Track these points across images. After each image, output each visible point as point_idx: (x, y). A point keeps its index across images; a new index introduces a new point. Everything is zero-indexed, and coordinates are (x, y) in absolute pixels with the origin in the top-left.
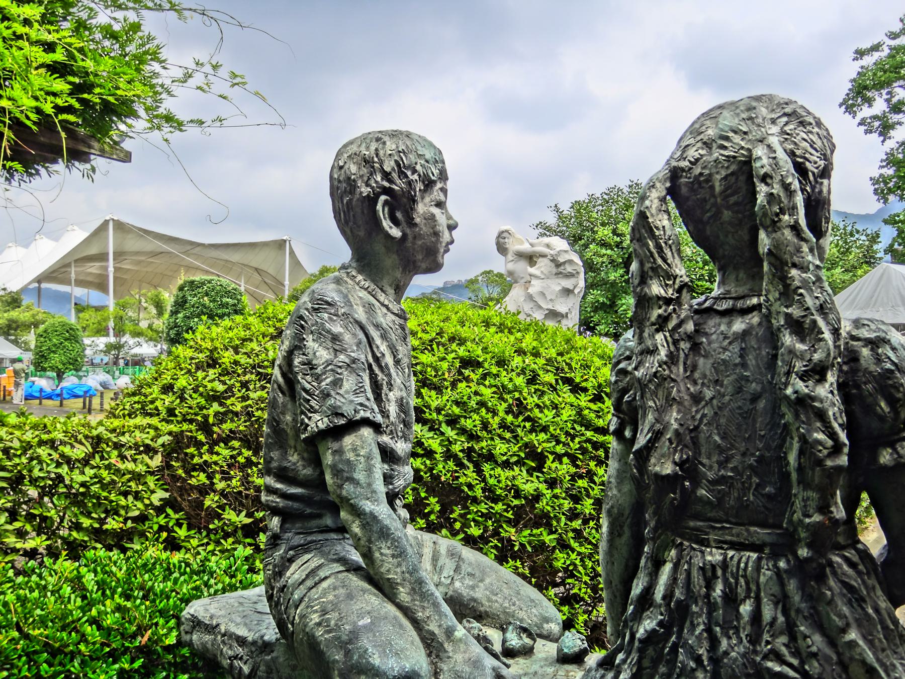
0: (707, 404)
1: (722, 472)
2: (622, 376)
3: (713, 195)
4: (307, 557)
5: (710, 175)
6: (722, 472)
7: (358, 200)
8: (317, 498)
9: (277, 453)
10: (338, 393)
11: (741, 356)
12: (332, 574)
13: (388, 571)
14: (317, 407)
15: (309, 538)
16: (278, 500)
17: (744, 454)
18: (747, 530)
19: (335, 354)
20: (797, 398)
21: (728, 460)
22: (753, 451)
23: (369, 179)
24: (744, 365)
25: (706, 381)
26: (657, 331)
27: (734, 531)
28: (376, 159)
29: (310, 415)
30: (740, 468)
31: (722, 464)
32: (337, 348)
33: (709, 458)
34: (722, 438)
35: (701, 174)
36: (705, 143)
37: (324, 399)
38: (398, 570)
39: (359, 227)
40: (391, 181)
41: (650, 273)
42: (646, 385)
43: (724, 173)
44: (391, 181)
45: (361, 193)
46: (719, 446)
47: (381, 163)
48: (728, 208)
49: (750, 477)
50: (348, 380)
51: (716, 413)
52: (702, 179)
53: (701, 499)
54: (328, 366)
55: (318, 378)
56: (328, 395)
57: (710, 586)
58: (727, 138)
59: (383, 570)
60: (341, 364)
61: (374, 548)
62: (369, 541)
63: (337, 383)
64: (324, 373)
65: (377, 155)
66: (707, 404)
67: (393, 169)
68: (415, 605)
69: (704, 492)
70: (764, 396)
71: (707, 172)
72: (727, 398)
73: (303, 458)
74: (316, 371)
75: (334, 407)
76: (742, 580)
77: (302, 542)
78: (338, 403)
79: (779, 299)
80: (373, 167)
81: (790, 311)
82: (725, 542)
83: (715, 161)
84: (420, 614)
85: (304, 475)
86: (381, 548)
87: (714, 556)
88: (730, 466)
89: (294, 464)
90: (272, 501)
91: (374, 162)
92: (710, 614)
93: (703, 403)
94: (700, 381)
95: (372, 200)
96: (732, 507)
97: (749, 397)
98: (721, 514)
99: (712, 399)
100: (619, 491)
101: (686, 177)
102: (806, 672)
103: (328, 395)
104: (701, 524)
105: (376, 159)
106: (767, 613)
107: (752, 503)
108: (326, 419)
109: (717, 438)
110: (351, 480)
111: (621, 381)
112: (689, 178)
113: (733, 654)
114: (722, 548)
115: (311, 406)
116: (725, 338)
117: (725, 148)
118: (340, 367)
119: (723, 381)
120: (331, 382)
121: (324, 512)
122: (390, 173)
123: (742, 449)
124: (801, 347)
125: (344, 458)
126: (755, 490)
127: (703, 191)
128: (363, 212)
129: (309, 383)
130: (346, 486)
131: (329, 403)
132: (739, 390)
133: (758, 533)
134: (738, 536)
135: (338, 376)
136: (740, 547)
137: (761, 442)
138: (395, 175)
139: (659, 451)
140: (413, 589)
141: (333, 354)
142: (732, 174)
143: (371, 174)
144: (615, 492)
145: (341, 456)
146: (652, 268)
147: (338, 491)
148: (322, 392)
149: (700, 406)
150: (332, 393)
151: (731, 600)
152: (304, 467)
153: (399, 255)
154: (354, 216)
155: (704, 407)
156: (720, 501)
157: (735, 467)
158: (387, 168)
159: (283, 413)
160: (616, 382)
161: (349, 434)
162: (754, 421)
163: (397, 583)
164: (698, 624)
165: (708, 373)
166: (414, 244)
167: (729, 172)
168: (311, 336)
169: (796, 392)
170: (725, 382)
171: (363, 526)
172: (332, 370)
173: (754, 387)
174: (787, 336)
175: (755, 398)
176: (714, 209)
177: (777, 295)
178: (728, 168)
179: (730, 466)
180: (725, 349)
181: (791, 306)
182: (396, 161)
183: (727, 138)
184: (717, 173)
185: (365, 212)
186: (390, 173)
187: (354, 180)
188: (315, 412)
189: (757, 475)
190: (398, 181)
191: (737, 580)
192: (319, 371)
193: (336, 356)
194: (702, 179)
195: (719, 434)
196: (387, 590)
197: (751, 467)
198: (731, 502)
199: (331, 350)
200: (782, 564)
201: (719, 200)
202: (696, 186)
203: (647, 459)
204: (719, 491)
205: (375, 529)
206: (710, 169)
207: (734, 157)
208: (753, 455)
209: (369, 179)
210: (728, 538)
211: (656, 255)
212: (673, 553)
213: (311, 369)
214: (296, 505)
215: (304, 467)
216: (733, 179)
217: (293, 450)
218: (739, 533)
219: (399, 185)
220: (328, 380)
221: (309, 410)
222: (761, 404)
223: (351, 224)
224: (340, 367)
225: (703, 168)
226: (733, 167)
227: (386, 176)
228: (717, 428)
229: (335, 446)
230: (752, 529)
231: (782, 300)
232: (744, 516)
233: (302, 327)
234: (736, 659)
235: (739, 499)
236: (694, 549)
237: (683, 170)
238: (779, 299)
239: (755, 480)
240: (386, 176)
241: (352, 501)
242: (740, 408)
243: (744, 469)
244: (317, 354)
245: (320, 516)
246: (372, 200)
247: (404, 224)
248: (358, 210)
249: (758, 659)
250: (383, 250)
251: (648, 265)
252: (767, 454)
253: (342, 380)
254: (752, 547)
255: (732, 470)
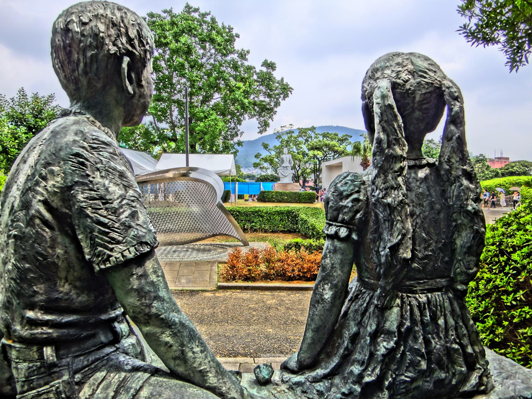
0: (417, 217)
1: (426, 253)
2: (356, 203)
3: (413, 102)
4: (100, 375)
5: (414, 91)
6: (426, 253)
7: (104, 55)
8: (92, 321)
9: (42, 286)
10: (138, 225)
11: (428, 190)
12: (144, 382)
13: (200, 364)
14: (120, 239)
15: (91, 358)
16: (50, 331)
17: (436, 242)
18: (435, 281)
19: (126, 190)
20: (475, 211)
21: (429, 246)
22: (440, 240)
23: (116, 40)
24: (430, 195)
25: (414, 204)
26: (399, 176)
27: (429, 283)
28: (122, 25)
29: (111, 246)
30: (435, 249)
31: (425, 249)
32: (126, 184)
33: (419, 246)
34: (426, 235)
35: (410, 89)
36: (409, 72)
37: (127, 231)
38: (206, 361)
39: (99, 79)
40: (133, 46)
41: (394, 142)
42: (395, 208)
43: (424, 91)
44: (133, 46)
45: (109, 50)
46: (425, 239)
47: (127, 29)
48: (420, 110)
49: (439, 254)
50: (141, 212)
51: (422, 222)
52: (410, 92)
53: (414, 269)
54: (122, 200)
55: (115, 212)
56: (130, 227)
57: (422, 315)
58: (426, 73)
59: (195, 365)
60: (133, 198)
61: (187, 350)
62: (182, 345)
63: (134, 215)
64: (121, 207)
65: (123, 21)
66: (417, 217)
67: (136, 36)
68: (220, 383)
69: (416, 265)
70: (442, 211)
71: (412, 88)
72: (427, 213)
73: (75, 287)
74: (113, 205)
75: (139, 237)
76: (439, 307)
77: (86, 363)
78: (140, 233)
79: (459, 161)
80: (120, 31)
81: (465, 167)
82: (425, 290)
83: (418, 83)
84: (224, 388)
85: (80, 302)
86: (193, 348)
87: (423, 299)
88: (430, 249)
89: (67, 294)
90: (42, 333)
91: (120, 27)
92: (424, 329)
93: (415, 216)
94: (411, 204)
95: (118, 58)
96: (430, 270)
97: (436, 212)
98: (424, 275)
99: (420, 214)
100: (342, 272)
101: (401, 89)
102: (462, 344)
103: (130, 227)
104: (413, 282)
105: (122, 25)
106: (451, 322)
107: (440, 267)
108: (132, 249)
109: (424, 235)
110: (157, 298)
111: (355, 206)
112: (403, 90)
113: (438, 346)
114: (424, 293)
115: (110, 238)
116: (417, 181)
117: (425, 78)
118: (133, 201)
119: (423, 204)
120: (129, 215)
121: (97, 331)
122: (134, 39)
123: (436, 239)
124: (472, 186)
125: (149, 280)
126: (441, 260)
127: (409, 98)
128: (107, 67)
129: (105, 217)
130: (155, 304)
131: (132, 233)
132: (432, 208)
133: (441, 282)
134: (431, 285)
135: (134, 209)
136: (431, 291)
137: (444, 235)
138: (136, 42)
139: (404, 245)
140: (217, 372)
141: (123, 189)
142: (430, 92)
143: (118, 36)
144: (339, 272)
145: (146, 279)
146: (395, 139)
147: (147, 310)
148: (123, 224)
149: (414, 218)
150: (133, 224)
151: (434, 318)
152: (78, 295)
153: (124, 108)
154: (97, 68)
155: (416, 219)
156: (424, 268)
157: (433, 249)
158: (132, 36)
159: (53, 247)
160: (352, 206)
161: (149, 260)
162: (440, 224)
163: (207, 372)
164: (420, 337)
165: (414, 200)
166: (139, 101)
167: (428, 91)
168: (98, 173)
169: (474, 209)
170: (424, 205)
171: (174, 335)
172: (128, 204)
173: (438, 206)
174: (464, 181)
175: (439, 213)
176: (411, 110)
177: (458, 159)
178: (427, 88)
179: (430, 249)
180: (419, 187)
181: (465, 165)
182: (137, 30)
183: (426, 73)
184: (419, 90)
185: (109, 66)
186: (134, 39)
187: (103, 38)
188: (118, 242)
189: (442, 252)
190: (138, 48)
191: (436, 308)
192: (115, 204)
193: (127, 192)
194: (410, 92)
195: (425, 233)
196: (197, 378)
197: (440, 248)
198: (429, 268)
199: (121, 186)
200: (451, 295)
201: (416, 105)
202: (406, 95)
203: (398, 251)
204: (424, 263)
205: (185, 334)
206: (414, 87)
207: (432, 84)
208: (441, 242)
209: (116, 40)
210: (426, 287)
211: (398, 132)
212: (398, 301)
213: (104, 204)
214: (72, 331)
215: (78, 295)
216: (429, 95)
217: (63, 281)
218: (432, 283)
219: (138, 51)
220: (126, 214)
221: (109, 242)
222: (442, 215)
223: (90, 75)
224: (133, 201)
225: (411, 86)
226: (431, 89)
227: (130, 40)
228: (423, 230)
229: (139, 271)
230: (438, 280)
231: (461, 162)
232: (435, 274)
233: (82, 164)
234: (440, 348)
235: (434, 266)
236: (410, 297)
237: (399, 84)
238: (459, 161)
239: (441, 255)
240: (130, 40)
241: (161, 316)
242: (434, 218)
243: (437, 250)
244: (110, 189)
245: (94, 336)
246: (118, 58)
247: (135, 84)
248: (103, 64)
249: (448, 345)
250: (114, 102)
251: (392, 137)
252: (447, 241)
253: (136, 212)
254: (439, 290)
255: (431, 251)
